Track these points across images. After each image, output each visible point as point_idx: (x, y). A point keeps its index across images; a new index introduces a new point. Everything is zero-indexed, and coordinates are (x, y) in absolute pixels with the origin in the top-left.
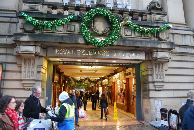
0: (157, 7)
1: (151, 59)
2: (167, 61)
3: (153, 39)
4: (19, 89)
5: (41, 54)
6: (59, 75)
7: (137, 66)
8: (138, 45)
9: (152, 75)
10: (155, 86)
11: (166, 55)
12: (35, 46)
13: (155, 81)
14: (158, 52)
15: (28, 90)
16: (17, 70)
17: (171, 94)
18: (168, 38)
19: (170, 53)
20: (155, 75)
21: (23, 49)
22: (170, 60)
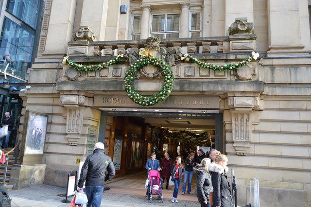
0: (240, 28)
3: (229, 79)
4: (64, 144)
5: (86, 104)
8: (202, 89)
9: (231, 131)
11: (249, 101)
12: (78, 95)
16: (60, 122)
17: (263, 162)
21: (66, 99)
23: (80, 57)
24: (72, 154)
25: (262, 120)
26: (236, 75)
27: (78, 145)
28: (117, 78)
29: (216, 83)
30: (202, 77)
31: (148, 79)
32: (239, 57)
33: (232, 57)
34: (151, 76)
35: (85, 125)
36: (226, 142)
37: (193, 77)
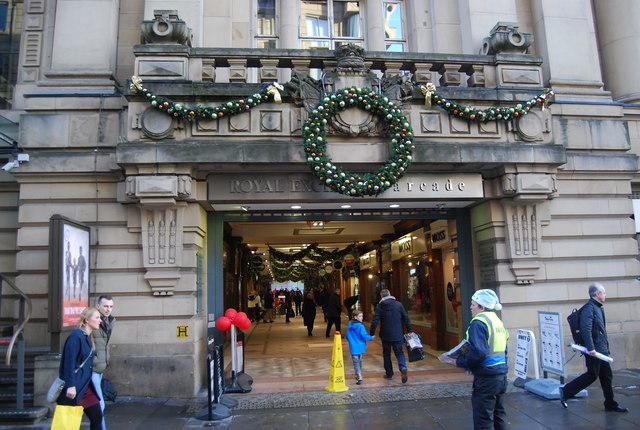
0: (513, 41)
1: (499, 194)
4: (138, 294)
5: (194, 196)
9: (503, 240)
10: (147, 281)
13: (146, 265)
21: (145, 185)
23: (173, 82)
24: (163, 317)
25: (556, 217)
26: (517, 132)
27: (176, 293)
28: (273, 134)
29: (485, 147)
30: (457, 135)
31: (346, 136)
32: (519, 97)
33: (508, 97)
34: (355, 130)
35: (187, 246)
36: (497, 262)
37: (277, 134)
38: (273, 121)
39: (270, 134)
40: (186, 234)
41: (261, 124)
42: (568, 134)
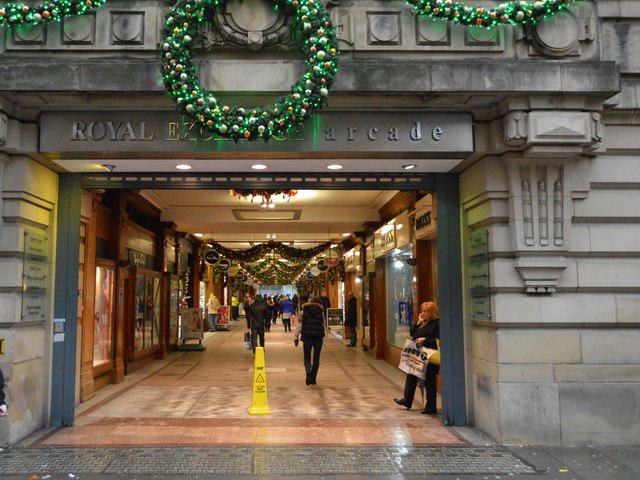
1: (498, 147)
2: (583, 155)
6: (152, 234)
7: (447, 187)
9: (505, 221)
10: (518, 270)
11: (575, 124)
13: (521, 247)
14: (532, 115)
15: (531, 294)
18: (588, 42)
19: (597, 116)
20: (519, 224)
22: (601, 147)
28: (129, 47)
34: (255, 38)
37: (88, 47)
38: (130, 27)
39: (123, 47)
40: (7, 202)
41: (112, 33)
42: (630, 48)
